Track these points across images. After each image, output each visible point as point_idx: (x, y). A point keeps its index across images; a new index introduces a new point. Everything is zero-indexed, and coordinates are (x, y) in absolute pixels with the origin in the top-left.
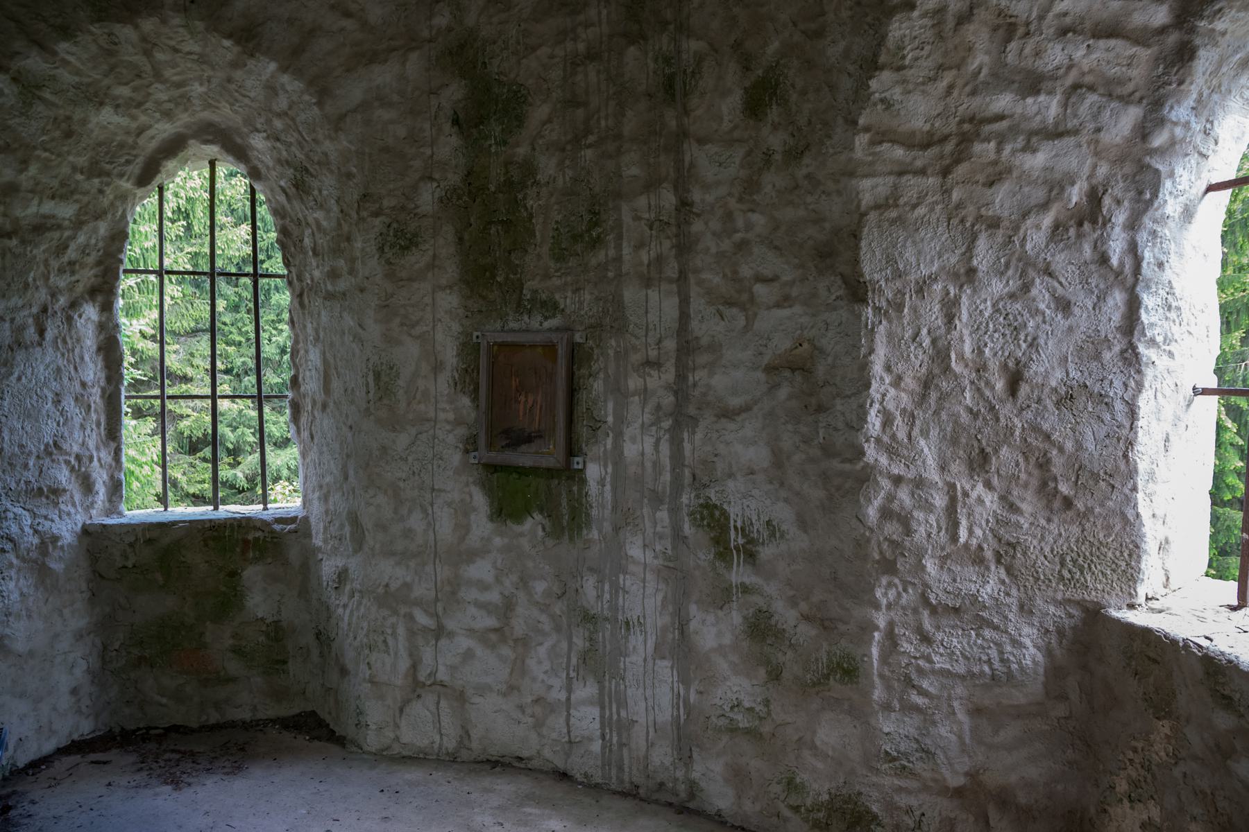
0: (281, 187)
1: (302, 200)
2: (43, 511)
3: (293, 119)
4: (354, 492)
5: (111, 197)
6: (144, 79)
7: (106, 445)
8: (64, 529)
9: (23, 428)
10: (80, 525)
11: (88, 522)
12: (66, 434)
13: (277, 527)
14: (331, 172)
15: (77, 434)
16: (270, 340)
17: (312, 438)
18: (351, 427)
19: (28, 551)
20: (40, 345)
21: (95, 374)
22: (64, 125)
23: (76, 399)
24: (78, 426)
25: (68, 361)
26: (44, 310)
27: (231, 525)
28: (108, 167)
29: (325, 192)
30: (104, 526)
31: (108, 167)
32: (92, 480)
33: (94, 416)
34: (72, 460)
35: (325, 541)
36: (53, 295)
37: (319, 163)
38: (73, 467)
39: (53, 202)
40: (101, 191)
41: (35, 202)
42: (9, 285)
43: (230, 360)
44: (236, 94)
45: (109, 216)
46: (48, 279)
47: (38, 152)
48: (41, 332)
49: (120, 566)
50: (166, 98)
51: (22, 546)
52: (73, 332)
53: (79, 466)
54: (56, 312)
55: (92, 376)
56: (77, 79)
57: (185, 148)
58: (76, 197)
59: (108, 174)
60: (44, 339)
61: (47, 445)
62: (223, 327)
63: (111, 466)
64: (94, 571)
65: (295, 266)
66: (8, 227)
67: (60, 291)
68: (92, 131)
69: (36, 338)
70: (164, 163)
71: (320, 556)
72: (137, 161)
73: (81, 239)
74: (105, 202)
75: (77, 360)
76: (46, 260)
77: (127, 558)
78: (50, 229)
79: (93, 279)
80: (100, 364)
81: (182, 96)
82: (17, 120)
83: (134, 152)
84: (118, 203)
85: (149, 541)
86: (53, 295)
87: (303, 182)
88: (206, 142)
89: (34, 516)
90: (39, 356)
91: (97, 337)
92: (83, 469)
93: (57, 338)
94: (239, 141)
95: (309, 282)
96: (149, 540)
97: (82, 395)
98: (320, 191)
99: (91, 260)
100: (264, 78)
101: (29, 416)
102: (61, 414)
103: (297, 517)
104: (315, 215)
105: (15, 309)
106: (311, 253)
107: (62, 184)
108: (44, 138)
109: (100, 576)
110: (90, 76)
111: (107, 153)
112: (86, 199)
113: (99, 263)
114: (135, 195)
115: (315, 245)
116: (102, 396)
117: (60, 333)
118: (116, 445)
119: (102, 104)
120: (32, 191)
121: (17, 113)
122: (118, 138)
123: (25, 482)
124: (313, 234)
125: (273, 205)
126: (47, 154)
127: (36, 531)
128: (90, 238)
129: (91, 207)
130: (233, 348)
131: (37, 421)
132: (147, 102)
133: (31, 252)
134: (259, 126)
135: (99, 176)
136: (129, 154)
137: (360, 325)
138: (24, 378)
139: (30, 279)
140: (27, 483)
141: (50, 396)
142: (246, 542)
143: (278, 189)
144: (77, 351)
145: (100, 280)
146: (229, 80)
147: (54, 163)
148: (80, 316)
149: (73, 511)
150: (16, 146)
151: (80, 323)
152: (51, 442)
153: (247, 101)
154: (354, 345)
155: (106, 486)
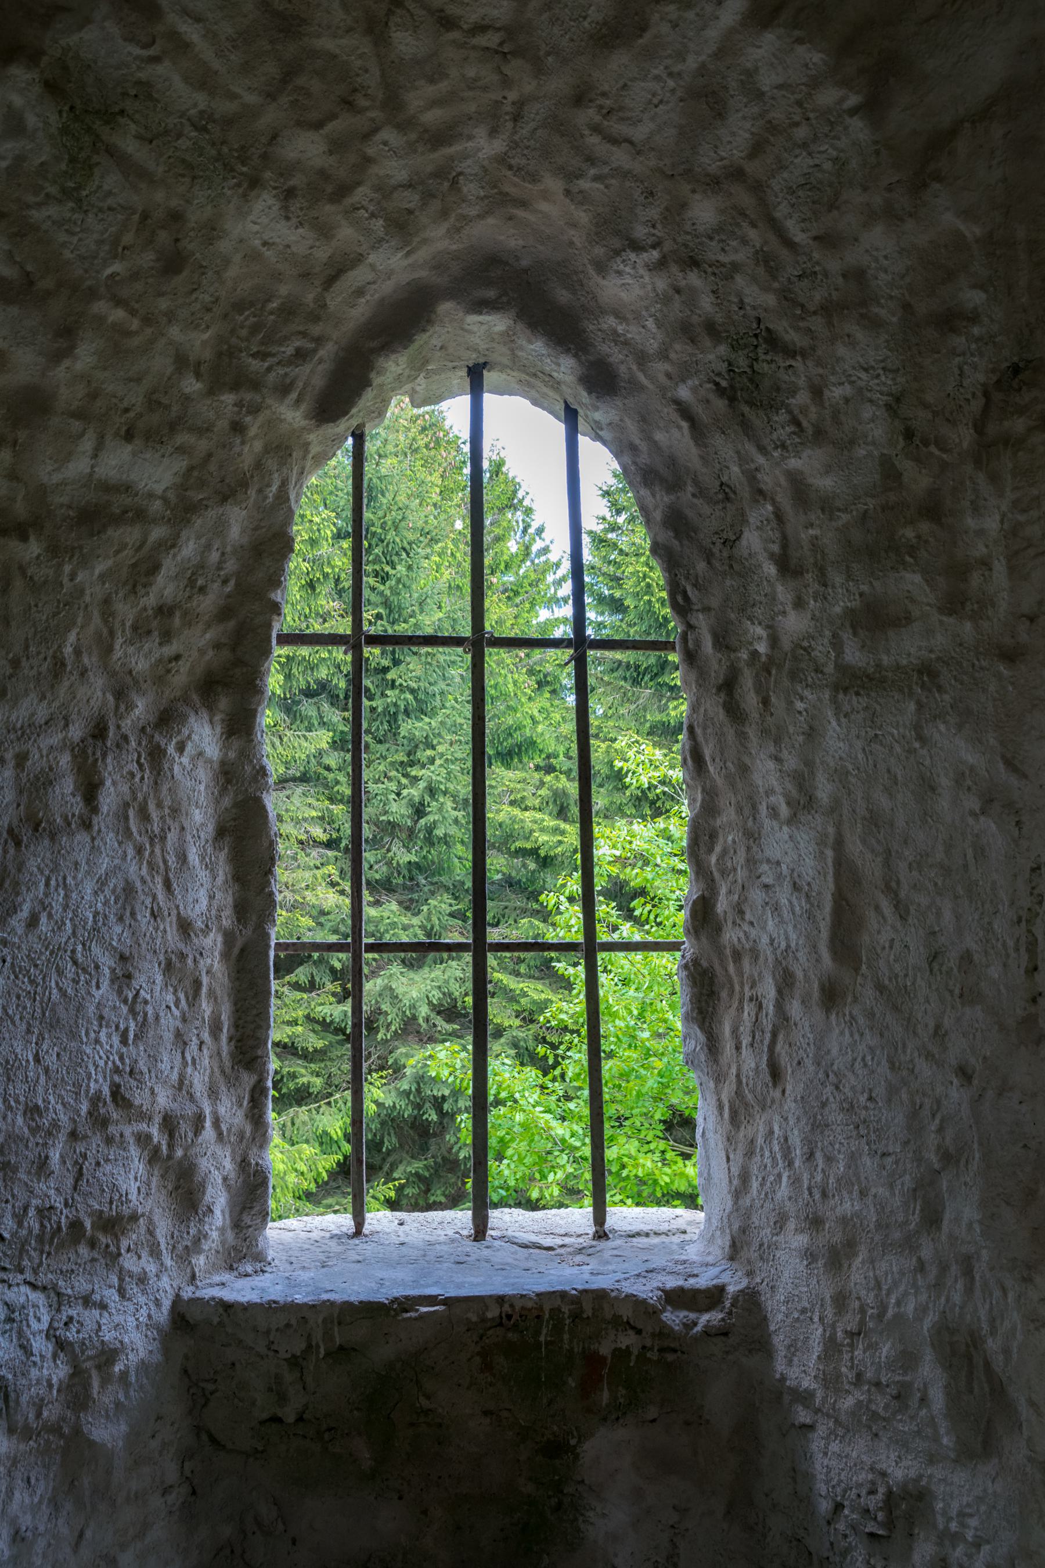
0: (677, 402)
1: (746, 426)
2: (81, 1284)
3: (758, 188)
4: (968, 1272)
5: (258, 446)
6: (361, 111)
7: (232, 1082)
8: (131, 1322)
9: (37, 1059)
10: (167, 1304)
11: (187, 1293)
12: (142, 1065)
13: (673, 1318)
14: (875, 324)
15: (168, 1063)
16: (398, 794)
17: (776, 1073)
18: (965, 1073)
19: (39, 1406)
20: (87, 825)
21: (212, 897)
22: (163, 237)
23: (168, 968)
24: (169, 1036)
25: (152, 867)
26: (99, 732)
27: (556, 1312)
28: (256, 365)
29: (836, 393)
30: (227, 1307)
31: (256, 365)
32: (198, 1178)
33: (206, 1008)
34: (155, 1131)
35: (831, 1381)
36: (120, 694)
37: (827, 310)
38: (157, 1150)
39: (129, 448)
40: (238, 428)
41: (87, 444)
42: (15, 663)
43: (336, 826)
44: (594, 140)
45: (252, 492)
46: (110, 649)
47: (100, 307)
48: (90, 791)
49: (265, 1416)
50: (402, 176)
51: (24, 1399)
52: (164, 789)
53: (171, 1146)
54: (125, 738)
55: (204, 902)
56: (201, 99)
57: (429, 321)
58: (183, 438)
59: (256, 385)
60: (95, 810)
61: (96, 1100)
62: (326, 773)
63: (241, 1135)
64: (198, 1430)
65: (707, 609)
66: (20, 509)
67: (136, 682)
68: (227, 261)
69: (77, 806)
70: (381, 362)
71: (803, 1416)
72: (322, 353)
73: (189, 549)
74: (249, 451)
75: (172, 860)
76: (107, 601)
77: (282, 1398)
78: (118, 520)
79: (211, 653)
80: (223, 871)
81: (439, 174)
82: (52, 211)
83: (316, 330)
84: (271, 463)
85: (343, 1352)
86: (120, 694)
87: (754, 378)
88: (480, 306)
89: (58, 1299)
90: (81, 857)
91: (217, 802)
92: (179, 1153)
93: (126, 805)
94: (563, 296)
95: (762, 648)
96: (341, 1348)
97: (182, 956)
98: (817, 392)
99: (207, 603)
100: (692, 63)
101: (54, 1024)
102: (133, 1011)
103: (721, 1289)
104: (794, 463)
105: (29, 730)
106: (770, 569)
107: (152, 403)
108: (116, 267)
109: (213, 1440)
110: (233, 96)
111: (255, 329)
112: (203, 445)
113: (225, 613)
114: (306, 446)
115: (785, 545)
116: (226, 955)
117: (133, 793)
118: (254, 1078)
119: (255, 183)
120: (79, 414)
121: (53, 190)
122: (284, 290)
123: (40, 1211)
124: (779, 516)
125: (644, 459)
126: (118, 314)
127: (61, 1345)
128: (208, 547)
129: (212, 467)
130: (341, 807)
131: (73, 1035)
132: (359, 184)
133: (72, 577)
134: (640, 232)
135: (235, 387)
136: (304, 334)
137: (1009, 763)
138: (44, 919)
139: (68, 650)
140: (45, 1212)
141: (107, 962)
142: (594, 1360)
143: (670, 412)
144: (172, 837)
145: (226, 654)
146: (580, 98)
147: (136, 342)
148: (181, 748)
149: (152, 1268)
150: (46, 284)
151: (180, 764)
152: (106, 1091)
153: (620, 157)
154: (988, 825)
155: (228, 1187)
